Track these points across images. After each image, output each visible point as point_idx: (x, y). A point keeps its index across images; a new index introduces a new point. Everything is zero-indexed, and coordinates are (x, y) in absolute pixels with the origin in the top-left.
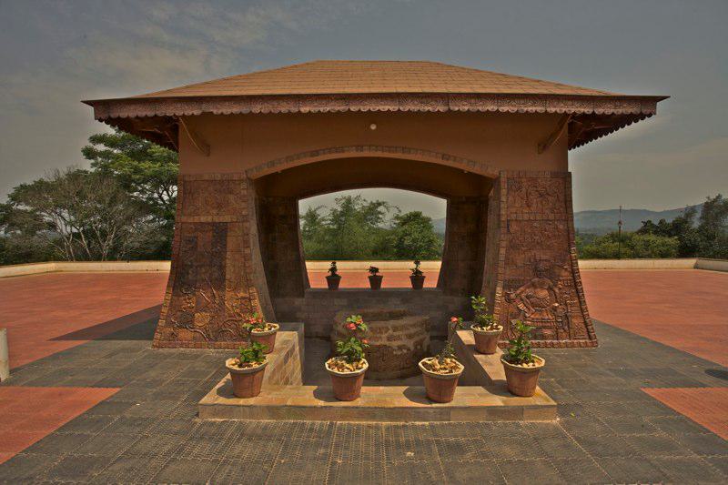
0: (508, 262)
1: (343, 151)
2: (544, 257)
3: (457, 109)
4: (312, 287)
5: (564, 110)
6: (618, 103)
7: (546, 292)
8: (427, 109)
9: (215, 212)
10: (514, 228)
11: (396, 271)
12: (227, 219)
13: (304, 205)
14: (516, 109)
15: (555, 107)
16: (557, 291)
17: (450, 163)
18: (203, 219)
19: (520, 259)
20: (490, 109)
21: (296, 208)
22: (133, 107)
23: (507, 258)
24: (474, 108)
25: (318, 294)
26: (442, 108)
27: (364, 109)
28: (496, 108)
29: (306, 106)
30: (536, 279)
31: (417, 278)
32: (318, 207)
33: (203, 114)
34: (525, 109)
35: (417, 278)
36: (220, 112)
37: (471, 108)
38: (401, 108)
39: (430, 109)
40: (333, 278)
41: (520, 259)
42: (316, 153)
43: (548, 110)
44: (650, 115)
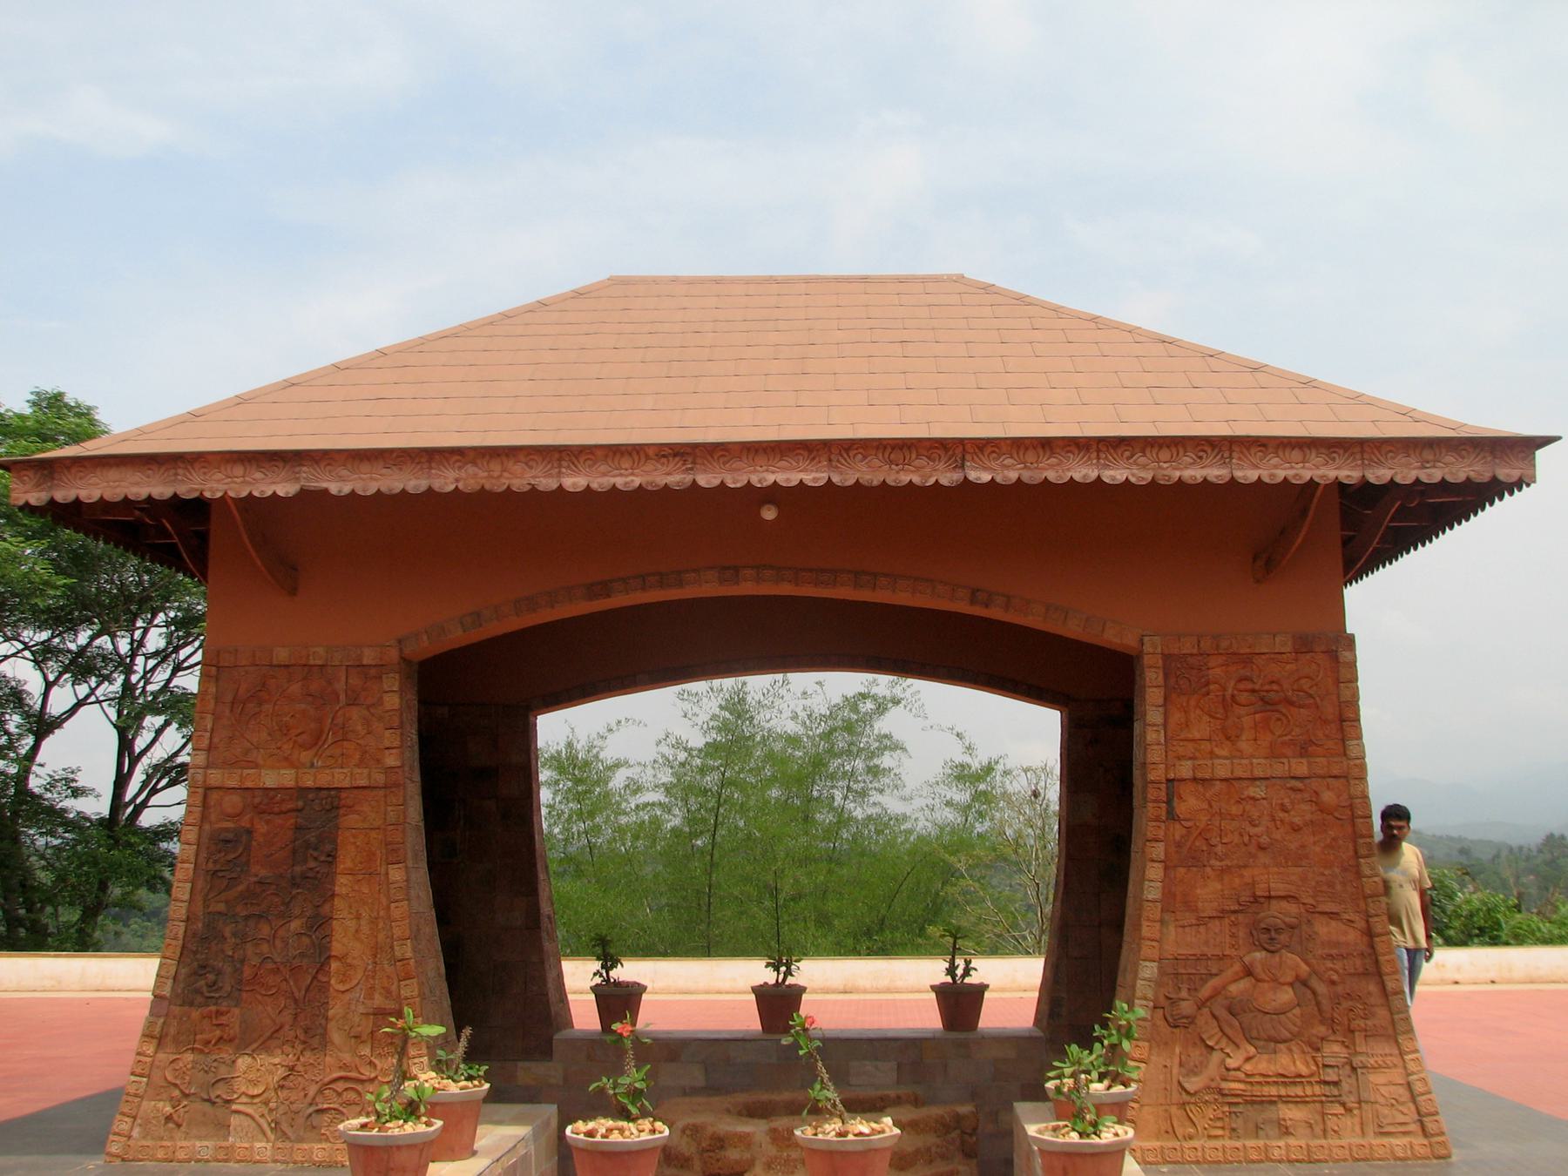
0: (1172, 901)
1: (680, 584)
2: (1279, 888)
3: (986, 477)
4: (576, 1026)
5: (1281, 474)
6: (1428, 455)
7: (1286, 995)
8: (905, 478)
9: (305, 756)
10: (1189, 803)
11: (870, 990)
12: (339, 777)
13: (554, 729)
14: (1148, 476)
15: (1256, 467)
16: (1321, 988)
17: (996, 613)
18: (270, 779)
19: (1209, 892)
20: (1077, 477)
21: (527, 734)
22: (113, 473)
23: (1168, 894)
24: (1032, 476)
25: (589, 1043)
26: (948, 478)
27: (735, 480)
28: (1093, 474)
29: (578, 473)
30: (1259, 955)
31: (960, 1001)
32: (623, 743)
33: (304, 494)
34: (1177, 474)
35: (960, 1001)
36: (346, 489)
37: (1027, 476)
38: (836, 479)
39: (916, 479)
40: (618, 1001)
41: (1209, 892)
42: (604, 589)
43: (1238, 474)
44: (1519, 484)
